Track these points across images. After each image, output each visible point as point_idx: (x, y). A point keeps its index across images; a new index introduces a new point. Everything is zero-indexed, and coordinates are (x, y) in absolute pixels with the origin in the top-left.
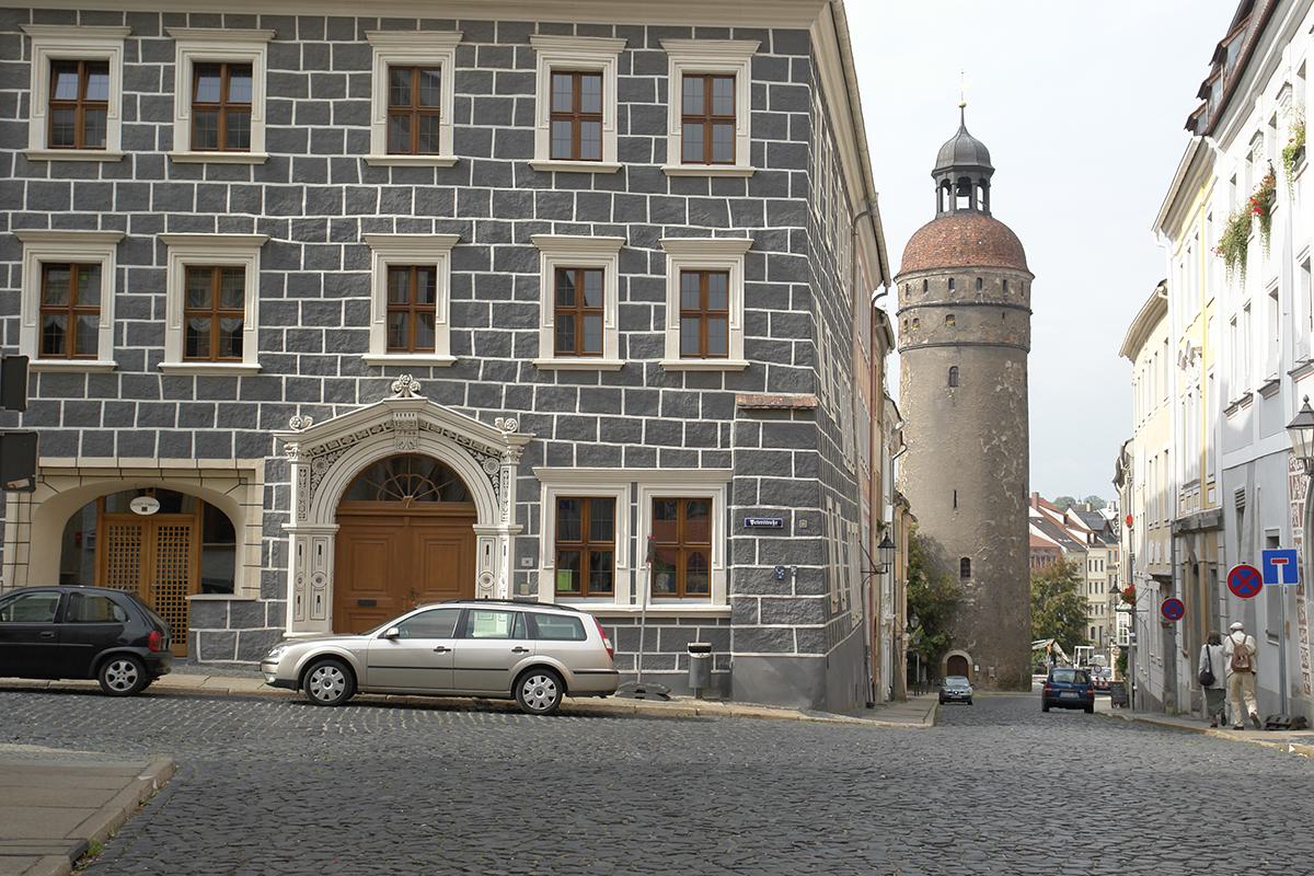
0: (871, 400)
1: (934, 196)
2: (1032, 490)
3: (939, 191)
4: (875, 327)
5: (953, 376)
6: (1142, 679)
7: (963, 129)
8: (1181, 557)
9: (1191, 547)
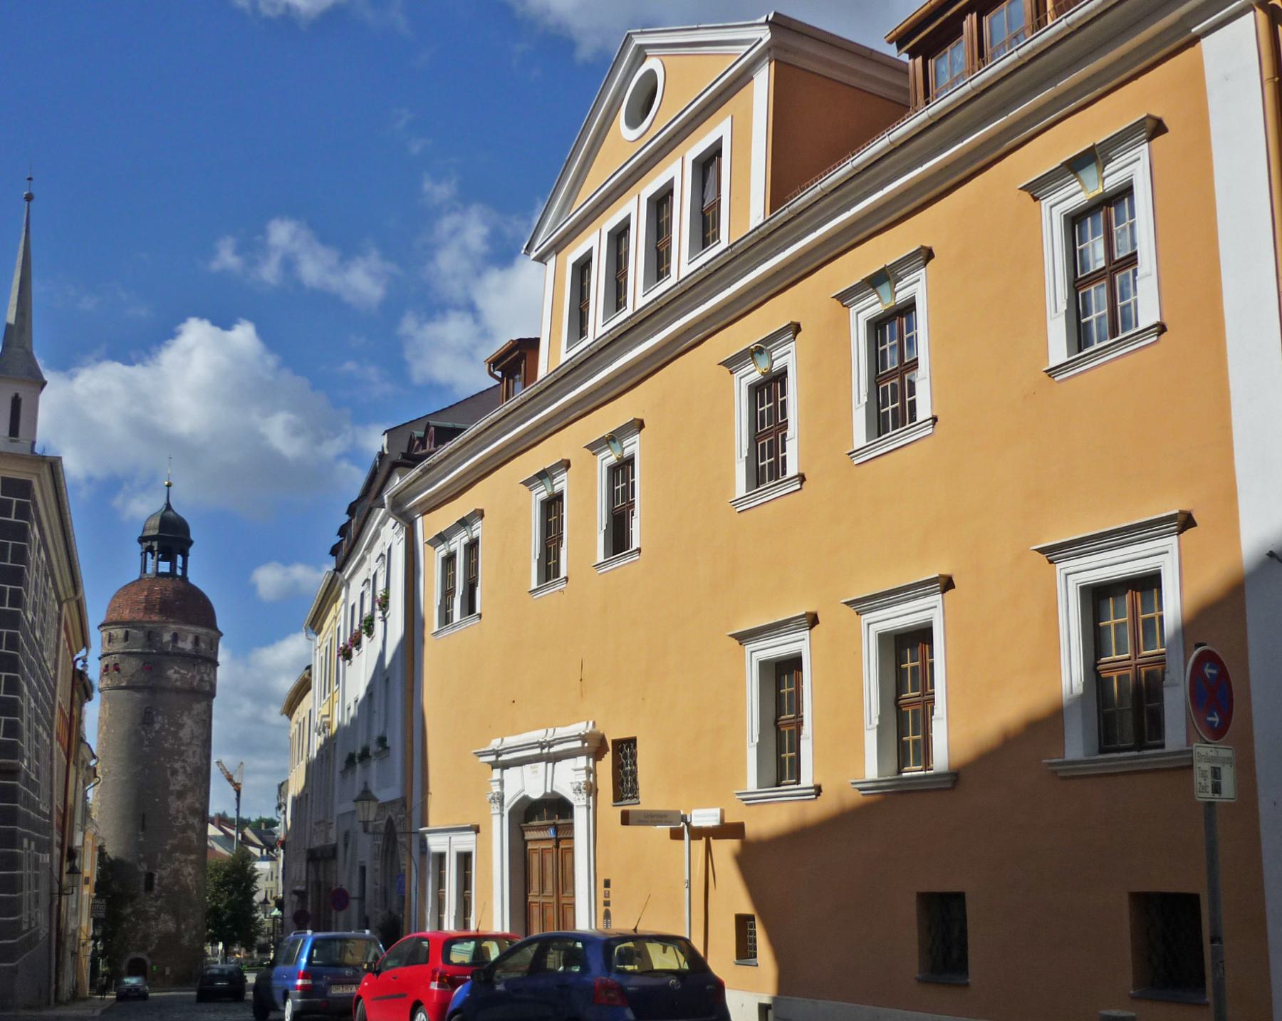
7: (168, 507)
8: (312, 878)
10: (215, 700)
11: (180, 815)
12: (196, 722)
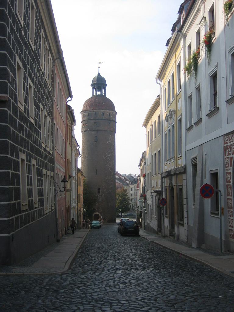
0: (66, 135)
1: (91, 91)
2: (116, 171)
4: (67, 111)
6: (149, 222)
7: (99, 74)
9: (171, 180)
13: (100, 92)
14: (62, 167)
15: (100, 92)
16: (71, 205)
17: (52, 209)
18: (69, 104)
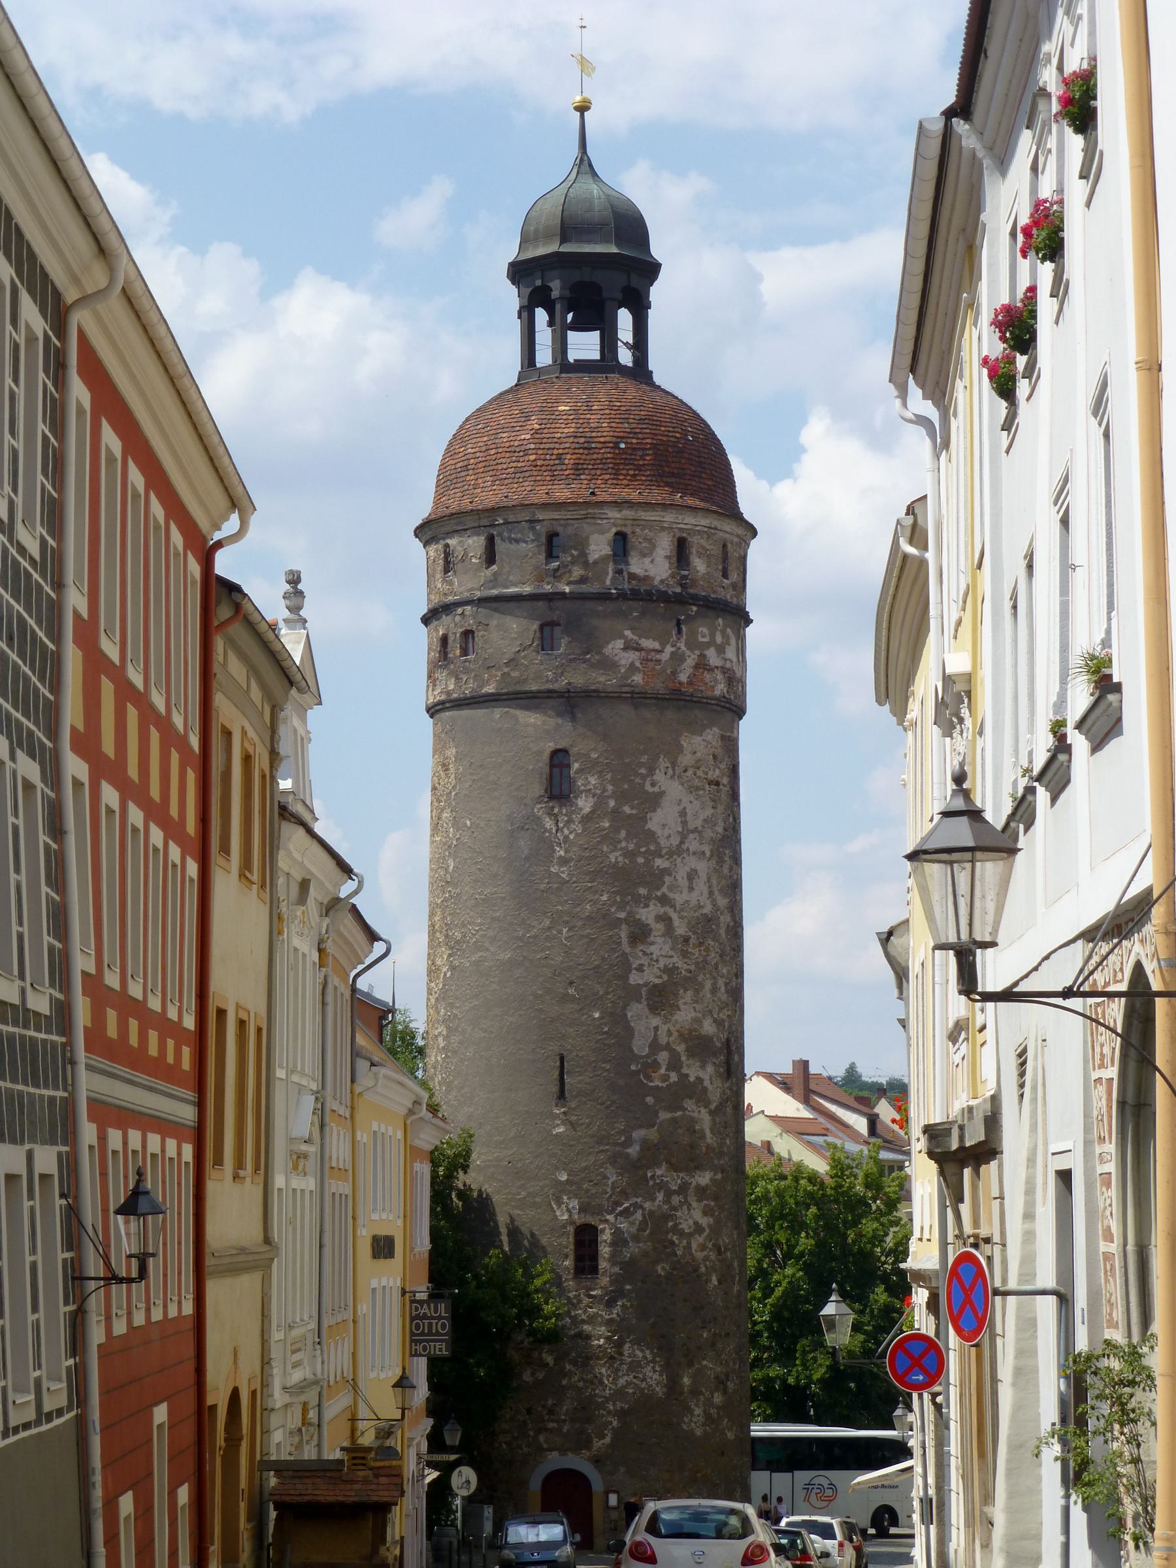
1: (515, 327)
3: (526, 314)
5: (558, 783)
7: (584, 164)
10: (746, 727)
11: (663, 1057)
12: (692, 789)
13: (594, 337)
14: (714, 508)
15: (594, 337)
16: (265, 1384)
17: (46, 1409)
18: (225, 565)
